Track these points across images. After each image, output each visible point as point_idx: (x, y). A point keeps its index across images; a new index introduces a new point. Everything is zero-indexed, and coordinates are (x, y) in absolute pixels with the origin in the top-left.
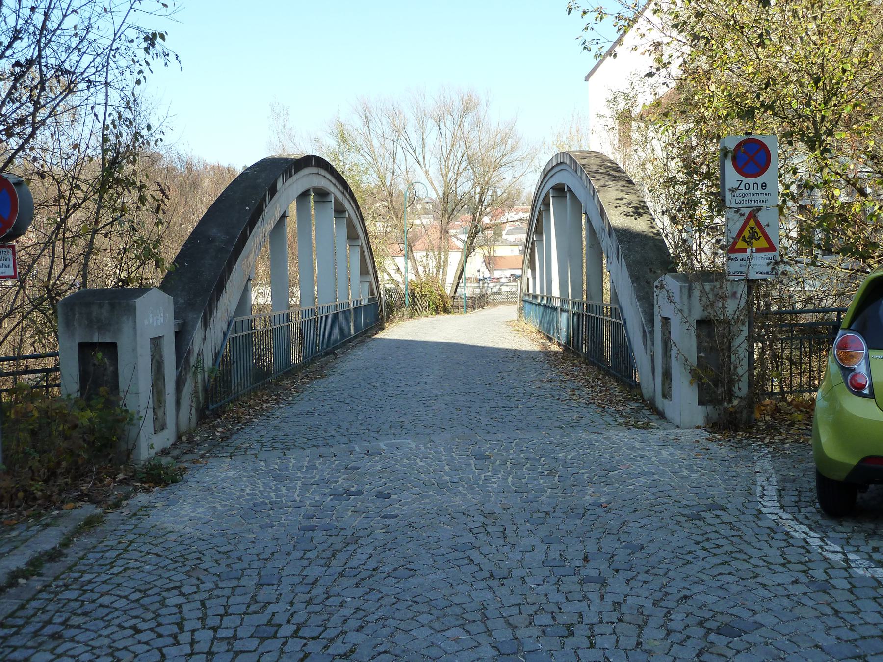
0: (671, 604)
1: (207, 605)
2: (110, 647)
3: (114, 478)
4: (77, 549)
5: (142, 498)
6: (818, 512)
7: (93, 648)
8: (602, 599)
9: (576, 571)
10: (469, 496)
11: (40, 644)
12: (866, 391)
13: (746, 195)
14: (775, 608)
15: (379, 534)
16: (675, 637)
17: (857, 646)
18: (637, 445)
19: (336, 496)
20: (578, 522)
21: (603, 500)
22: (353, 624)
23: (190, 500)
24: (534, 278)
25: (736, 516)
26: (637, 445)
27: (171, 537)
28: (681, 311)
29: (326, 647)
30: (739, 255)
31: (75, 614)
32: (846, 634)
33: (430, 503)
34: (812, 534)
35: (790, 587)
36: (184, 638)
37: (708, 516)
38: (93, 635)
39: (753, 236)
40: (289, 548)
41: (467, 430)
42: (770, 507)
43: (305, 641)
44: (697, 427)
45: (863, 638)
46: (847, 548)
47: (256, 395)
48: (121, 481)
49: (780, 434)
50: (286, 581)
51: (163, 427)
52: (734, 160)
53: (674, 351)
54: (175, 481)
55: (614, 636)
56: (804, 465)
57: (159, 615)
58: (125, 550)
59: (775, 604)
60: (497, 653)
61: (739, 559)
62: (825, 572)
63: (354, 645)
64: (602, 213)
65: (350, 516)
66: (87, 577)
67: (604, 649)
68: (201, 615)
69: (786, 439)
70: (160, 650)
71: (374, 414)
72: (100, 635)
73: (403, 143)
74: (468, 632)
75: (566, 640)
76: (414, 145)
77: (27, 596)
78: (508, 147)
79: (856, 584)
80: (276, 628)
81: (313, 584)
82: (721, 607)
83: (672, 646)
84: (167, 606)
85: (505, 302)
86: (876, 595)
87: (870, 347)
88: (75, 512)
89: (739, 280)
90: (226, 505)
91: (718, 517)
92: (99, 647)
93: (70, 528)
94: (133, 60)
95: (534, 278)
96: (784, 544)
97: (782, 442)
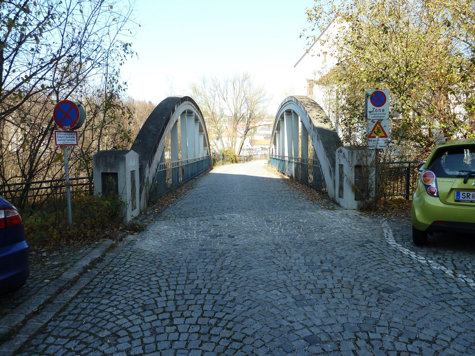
0: (361, 280)
1: (169, 281)
2: (133, 298)
3: (118, 229)
4: (109, 258)
5: (130, 237)
6: (412, 244)
7: (126, 298)
8: (333, 278)
9: (319, 267)
10: (267, 237)
11: (103, 296)
12: (435, 195)
13: (376, 114)
14: (404, 282)
15: (233, 252)
16: (366, 294)
17: (441, 297)
18: (331, 217)
19: (212, 237)
20: (315, 248)
21: (323, 239)
22: (232, 288)
23: (151, 238)
24: (276, 148)
25: (379, 245)
26: (331, 217)
27: (147, 253)
28: (349, 162)
29: (223, 298)
30: (373, 139)
31: (114, 284)
32: (435, 292)
33: (251, 240)
34: (411, 252)
35: (408, 274)
36: (163, 294)
37: (367, 245)
38: (124, 293)
39: (379, 131)
40: (197, 258)
41: (260, 210)
42: (392, 241)
43: (213, 295)
44: (354, 210)
45: (443, 294)
46: (427, 258)
47: (168, 195)
48: (120, 230)
49: (389, 212)
50: (199, 271)
51: (135, 208)
52: (371, 99)
53: (345, 179)
54: (143, 230)
55: (341, 293)
56: (401, 225)
57: (150, 285)
58: (129, 258)
59: (403, 280)
60: (295, 300)
61: (384, 263)
62: (421, 268)
63: (234, 297)
64: (311, 121)
65: (219, 245)
66: (115, 269)
67: (339, 298)
68: (167, 285)
69: (392, 214)
70: (154, 298)
71: (219, 204)
72: (127, 293)
73: (219, 92)
74: (281, 292)
75: (322, 295)
76: (223, 92)
77: (93, 277)
78: (262, 95)
79: (434, 272)
80: (200, 290)
81: (210, 272)
82: (382, 281)
83: (366, 297)
84: (152, 281)
85: (259, 159)
86: (444, 277)
87: (437, 176)
88: (104, 243)
89: (372, 149)
90: (166, 240)
91: (371, 246)
92: (128, 298)
93: (104, 249)
94: (118, 55)
95: (276, 148)
96: (401, 257)
97: (390, 215)
